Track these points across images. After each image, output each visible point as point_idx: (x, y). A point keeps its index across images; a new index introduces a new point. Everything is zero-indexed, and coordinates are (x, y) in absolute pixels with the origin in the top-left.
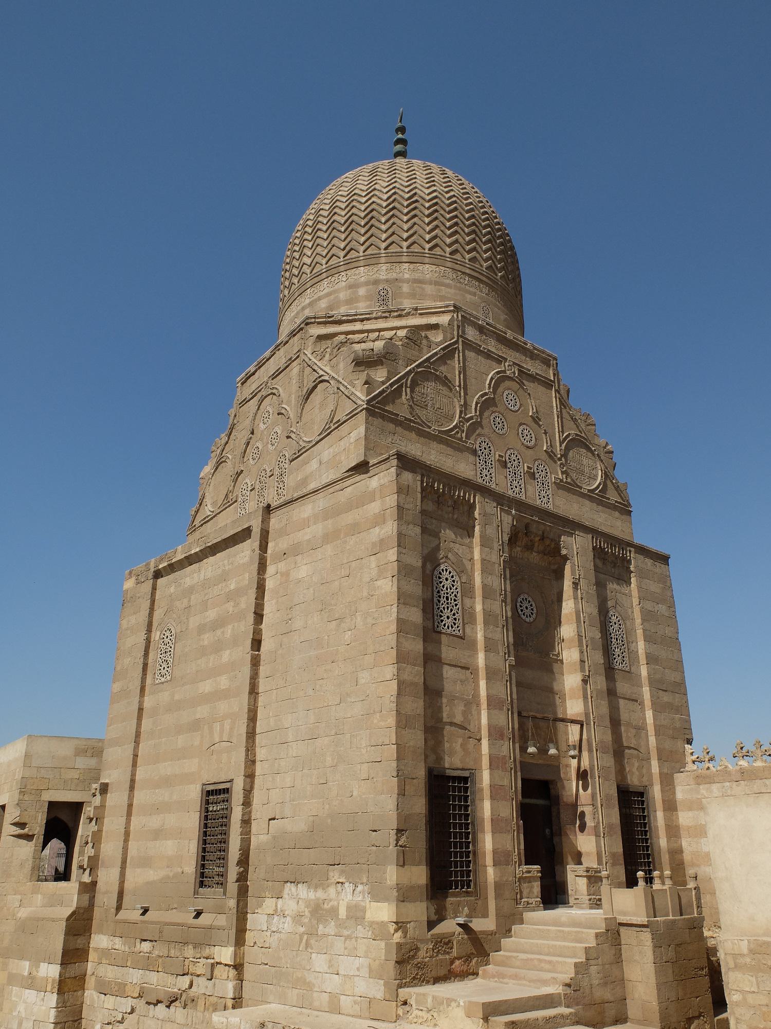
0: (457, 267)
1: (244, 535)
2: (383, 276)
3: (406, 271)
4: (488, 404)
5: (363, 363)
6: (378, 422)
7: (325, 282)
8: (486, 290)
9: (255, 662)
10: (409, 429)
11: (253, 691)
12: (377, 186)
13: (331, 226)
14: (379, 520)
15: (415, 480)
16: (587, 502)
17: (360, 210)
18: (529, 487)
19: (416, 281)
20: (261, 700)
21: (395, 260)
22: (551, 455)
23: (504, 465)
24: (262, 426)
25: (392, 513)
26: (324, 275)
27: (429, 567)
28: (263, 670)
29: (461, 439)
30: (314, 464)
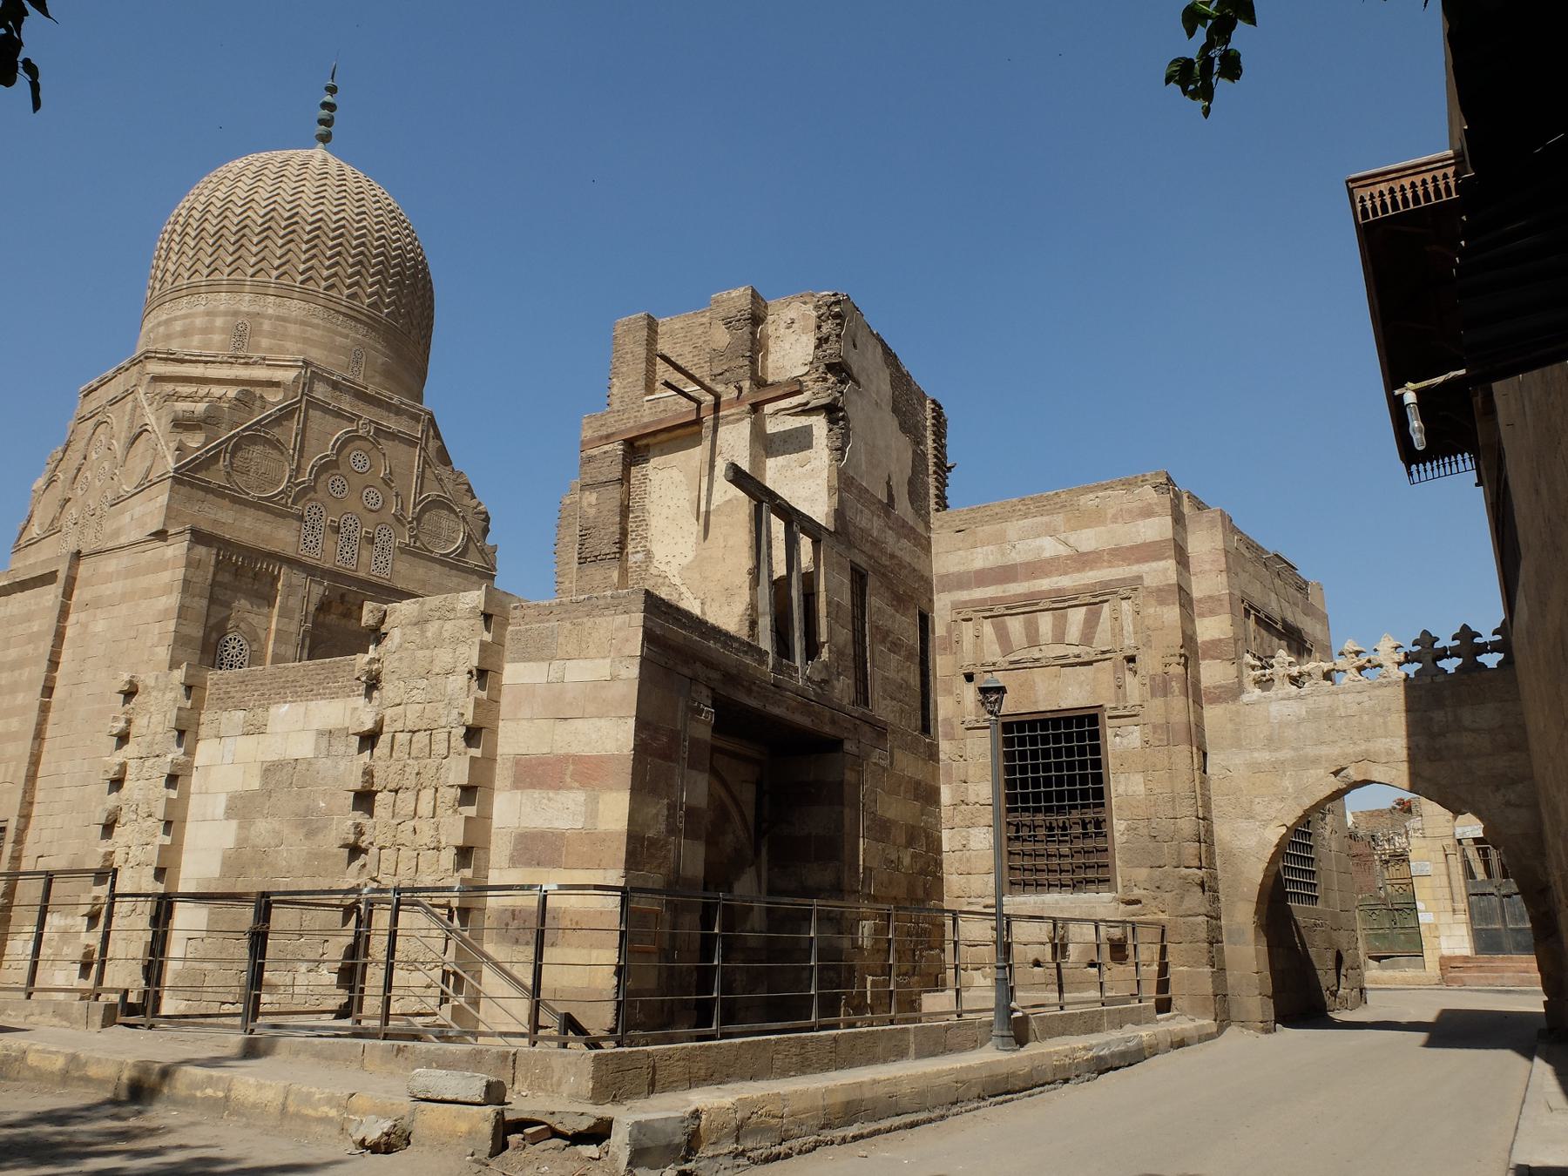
0: (331, 305)
1: (48, 579)
2: (244, 307)
3: (270, 306)
4: (326, 467)
5: (182, 424)
6: (185, 490)
7: (185, 300)
8: (362, 329)
9: (44, 709)
10: (223, 496)
11: (39, 736)
12: (256, 197)
13: (199, 237)
14: (167, 590)
15: (209, 554)
16: (437, 567)
17: (232, 222)
18: (364, 553)
19: (279, 318)
20: (46, 746)
21: (260, 291)
22: (399, 519)
23: (337, 530)
24: (94, 456)
25: (178, 585)
26: (184, 292)
27: (214, 636)
28: (52, 717)
29: (285, 505)
30: (127, 518)
